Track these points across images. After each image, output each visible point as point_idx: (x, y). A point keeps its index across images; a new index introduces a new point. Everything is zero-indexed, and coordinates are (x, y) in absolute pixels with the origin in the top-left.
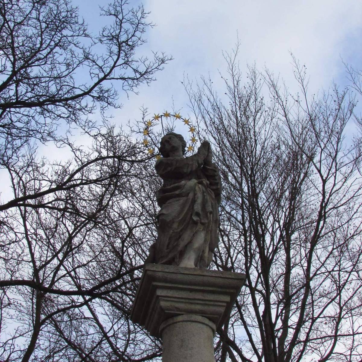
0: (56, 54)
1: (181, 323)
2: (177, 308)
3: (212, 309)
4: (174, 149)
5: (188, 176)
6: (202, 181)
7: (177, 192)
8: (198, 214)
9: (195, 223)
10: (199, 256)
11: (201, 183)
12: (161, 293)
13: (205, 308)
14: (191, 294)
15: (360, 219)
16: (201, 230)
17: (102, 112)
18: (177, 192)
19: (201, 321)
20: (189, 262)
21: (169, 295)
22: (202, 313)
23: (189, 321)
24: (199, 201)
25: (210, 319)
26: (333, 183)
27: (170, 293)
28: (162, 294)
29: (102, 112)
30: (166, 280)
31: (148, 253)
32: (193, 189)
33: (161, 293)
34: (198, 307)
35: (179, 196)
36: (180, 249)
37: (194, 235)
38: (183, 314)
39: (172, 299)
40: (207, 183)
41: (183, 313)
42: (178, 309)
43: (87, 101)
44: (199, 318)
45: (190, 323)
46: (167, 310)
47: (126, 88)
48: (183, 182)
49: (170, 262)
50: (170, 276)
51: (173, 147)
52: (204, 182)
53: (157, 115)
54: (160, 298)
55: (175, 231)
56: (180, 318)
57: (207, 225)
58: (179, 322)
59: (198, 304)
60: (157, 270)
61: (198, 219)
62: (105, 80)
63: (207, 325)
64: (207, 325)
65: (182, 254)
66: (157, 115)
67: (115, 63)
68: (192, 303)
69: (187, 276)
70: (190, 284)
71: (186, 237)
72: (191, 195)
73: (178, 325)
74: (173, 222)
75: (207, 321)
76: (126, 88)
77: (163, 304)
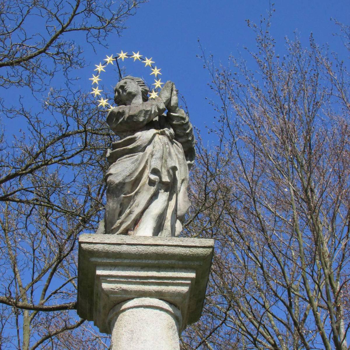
6: (164, 131)
7: (130, 147)
11: (163, 134)
15: (18, 1)
17: (65, 74)
18: (130, 147)
20: (145, 230)
22: (160, 295)
29: (65, 74)
31: (210, 277)
40: (170, 133)
42: (125, 291)
43: (46, 61)
44: (155, 302)
45: (142, 308)
47: (91, 39)
48: (138, 134)
51: (130, 93)
61: (157, 177)
64: (161, 309)
65: (136, 222)
67: (75, 12)
69: (135, 247)
72: (149, 149)
76: (91, 39)
77: (105, 286)
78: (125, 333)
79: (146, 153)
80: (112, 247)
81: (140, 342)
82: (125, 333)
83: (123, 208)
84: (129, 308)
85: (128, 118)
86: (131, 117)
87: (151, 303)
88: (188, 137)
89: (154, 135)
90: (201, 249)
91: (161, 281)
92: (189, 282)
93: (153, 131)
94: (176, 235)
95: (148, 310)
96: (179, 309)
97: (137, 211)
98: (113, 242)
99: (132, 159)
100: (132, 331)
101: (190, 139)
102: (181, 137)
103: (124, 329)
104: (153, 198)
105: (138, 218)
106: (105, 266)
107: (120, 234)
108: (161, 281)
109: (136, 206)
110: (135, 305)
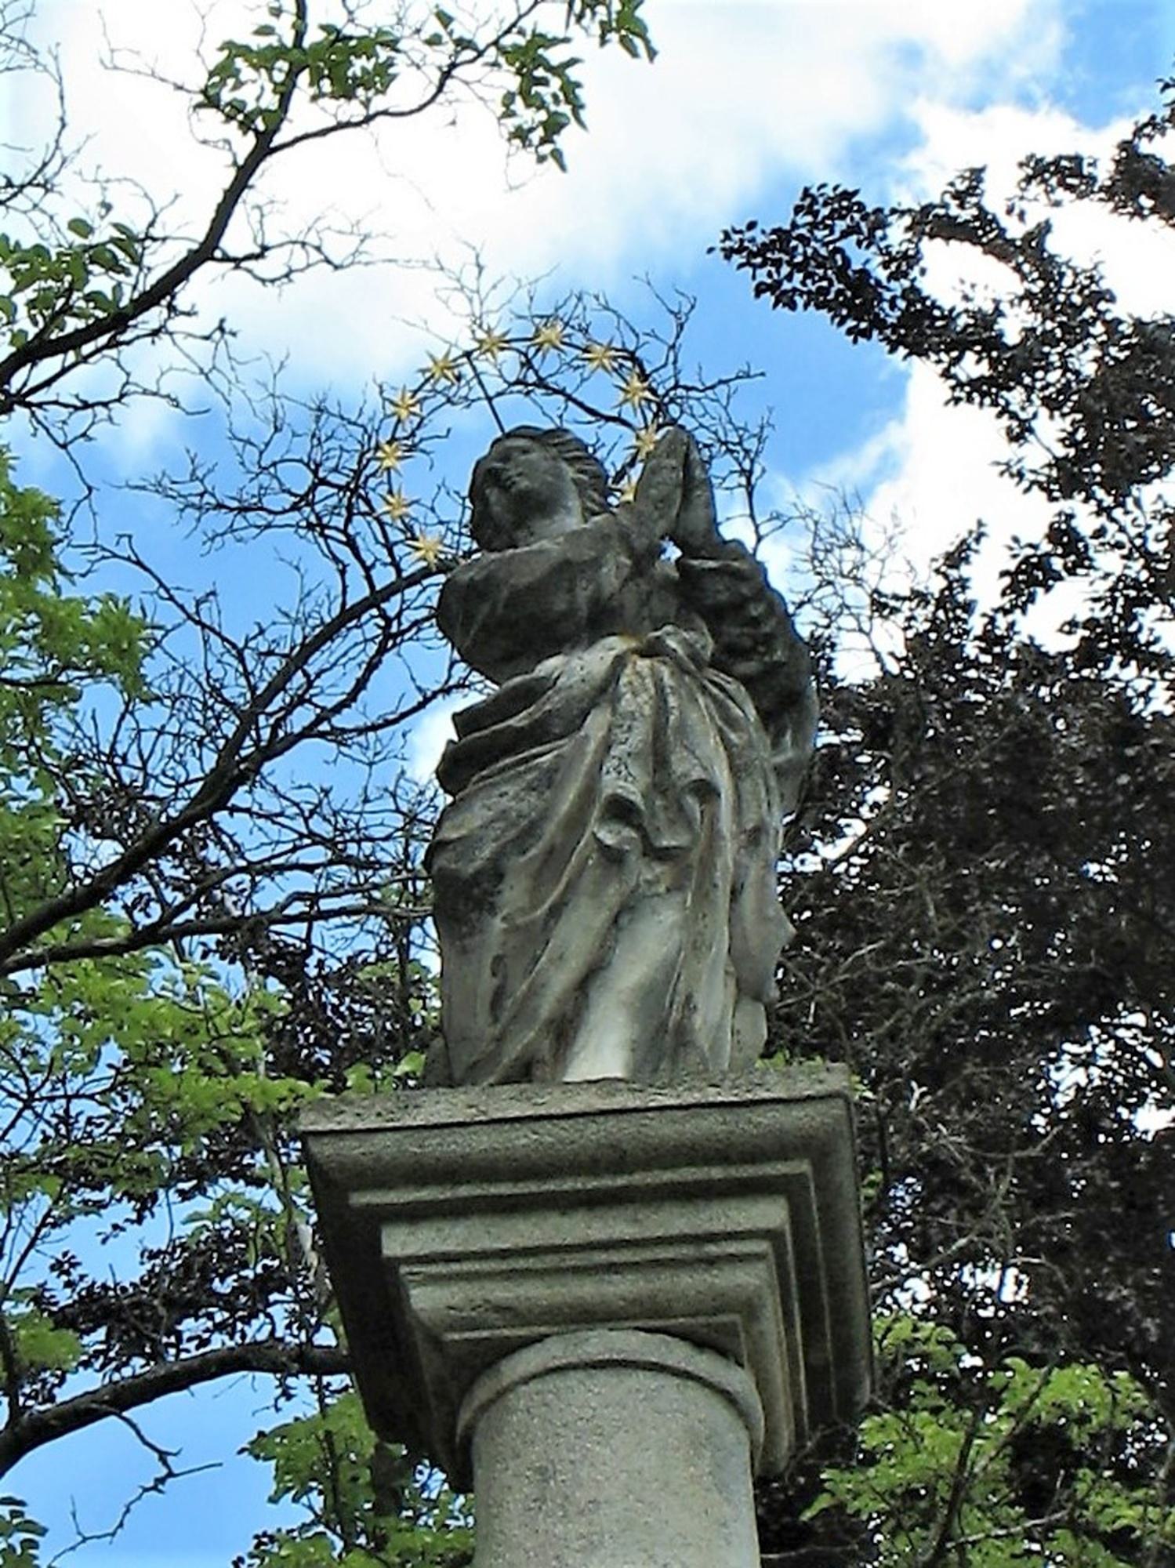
1: (534, 1386)
2: (499, 1309)
4: (534, 507)
8: (621, 810)
9: (613, 858)
10: (662, 1027)
11: (653, 651)
12: (404, 1245)
13: (663, 1283)
16: (662, 889)
19: (637, 1357)
20: (603, 1053)
21: (450, 1247)
22: (648, 1315)
23: (574, 1367)
25: (700, 1342)
26: (200, 233)
28: (411, 1250)
33: (404, 1245)
35: (538, 734)
36: (547, 1007)
38: (540, 1339)
39: (466, 1267)
41: (543, 1330)
46: (452, 1328)
48: (550, 665)
49: (524, 1072)
52: (672, 643)
53: (440, 357)
54: (404, 1270)
55: (520, 921)
57: (694, 857)
59: (733, 1258)
60: (360, 1126)
61: (629, 833)
63: (687, 1375)
64: (687, 1375)
65: (565, 1030)
66: (440, 357)
68: (711, 1262)
71: (577, 935)
72: (596, 724)
73: (520, 1399)
74: (495, 873)
75: (679, 1354)
78: (514, 1482)
79: (587, 737)
80: (797, 1112)
82: (514, 1482)
83: (505, 977)
84: (526, 1381)
86: (517, 597)
87: (611, 1350)
88: (771, 650)
89: (619, 662)
90: (810, 1109)
91: (647, 1255)
95: (601, 1376)
96: (741, 1365)
97: (560, 981)
98: (434, 1120)
99: (530, 770)
100: (541, 1471)
102: (745, 654)
103: (512, 1464)
104: (624, 920)
105: (569, 1008)
106: (413, 1215)
108: (647, 1255)
109: (550, 961)
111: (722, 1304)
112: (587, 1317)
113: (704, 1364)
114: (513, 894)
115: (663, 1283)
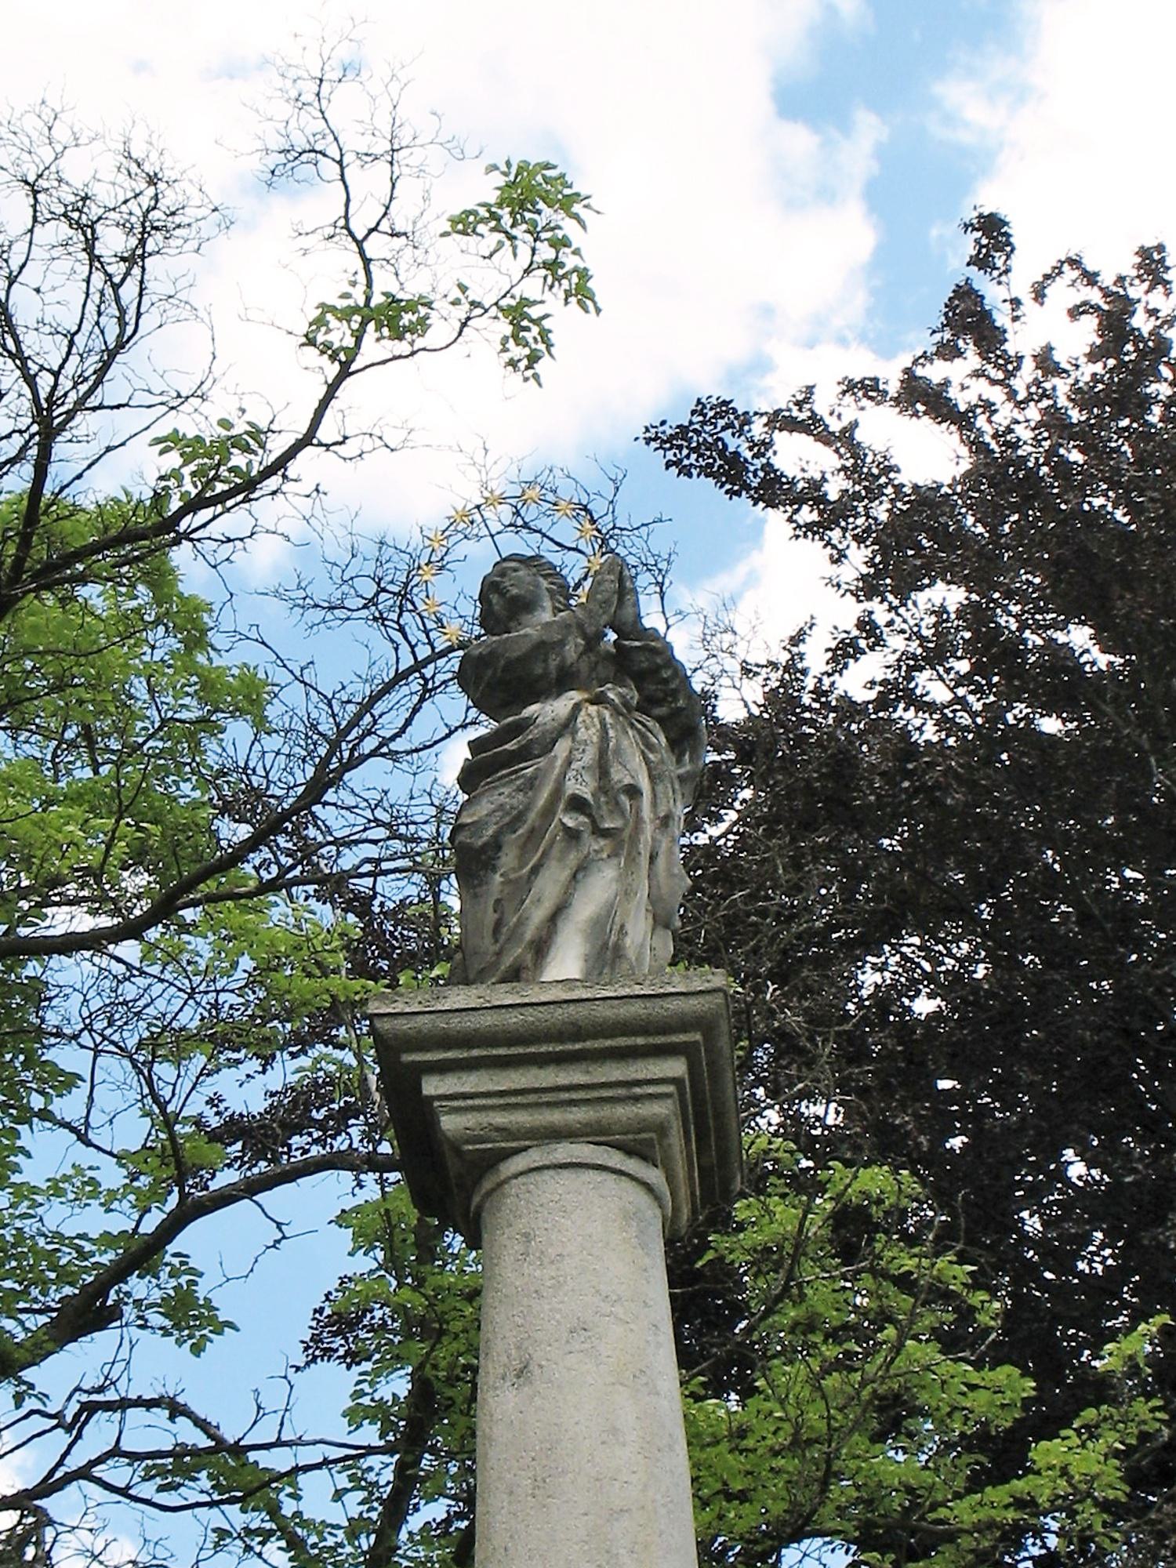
0: (309, 132)
2: (498, 1129)
3: (623, 1112)
5: (564, 681)
8: (577, 804)
9: (573, 835)
10: (605, 946)
11: (599, 700)
12: (436, 1087)
13: (606, 1113)
14: (562, 1074)
16: (605, 856)
19: (588, 1161)
20: (566, 963)
21: (467, 1089)
24: (589, 756)
25: (629, 1151)
27: (470, 1082)
28: (442, 1090)
30: (446, 1041)
32: (568, 726)
33: (436, 1087)
34: (578, 1116)
35: (524, 754)
36: (529, 933)
37: (574, 876)
39: (477, 1102)
41: (527, 1143)
42: (505, 1132)
46: (468, 1142)
48: (532, 710)
49: (514, 975)
50: (456, 1023)
52: (611, 695)
53: (460, 509)
55: (512, 876)
56: (518, 1163)
57: (626, 834)
58: (510, 1178)
61: (583, 819)
62: (349, 380)
65: (541, 948)
66: (460, 509)
69: (515, 1012)
70: (559, 1036)
71: (549, 886)
72: (562, 748)
74: (496, 845)
75: (616, 1159)
81: (546, 1261)
82: (507, 1243)
83: (502, 913)
84: (516, 1176)
85: (505, 669)
86: (510, 665)
88: (676, 700)
89: (577, 708)
92: (671, 1089)
93: (575, 696)
94: (471, 977)
95: (565, 1173)
97: (538, 915)
98: (456, 1006)
100: (526, 1235)
101: (681, 703)
102: (659, 702)
104: (580, 876)
105: (544, 933)
107: (503, 981)
109: (532, 902)
110: (532, 1166)
111: (644, 1125)
112: (556, 1134)
113: (632, 1165)
114: (508, 859)
115: (606, 1113)
